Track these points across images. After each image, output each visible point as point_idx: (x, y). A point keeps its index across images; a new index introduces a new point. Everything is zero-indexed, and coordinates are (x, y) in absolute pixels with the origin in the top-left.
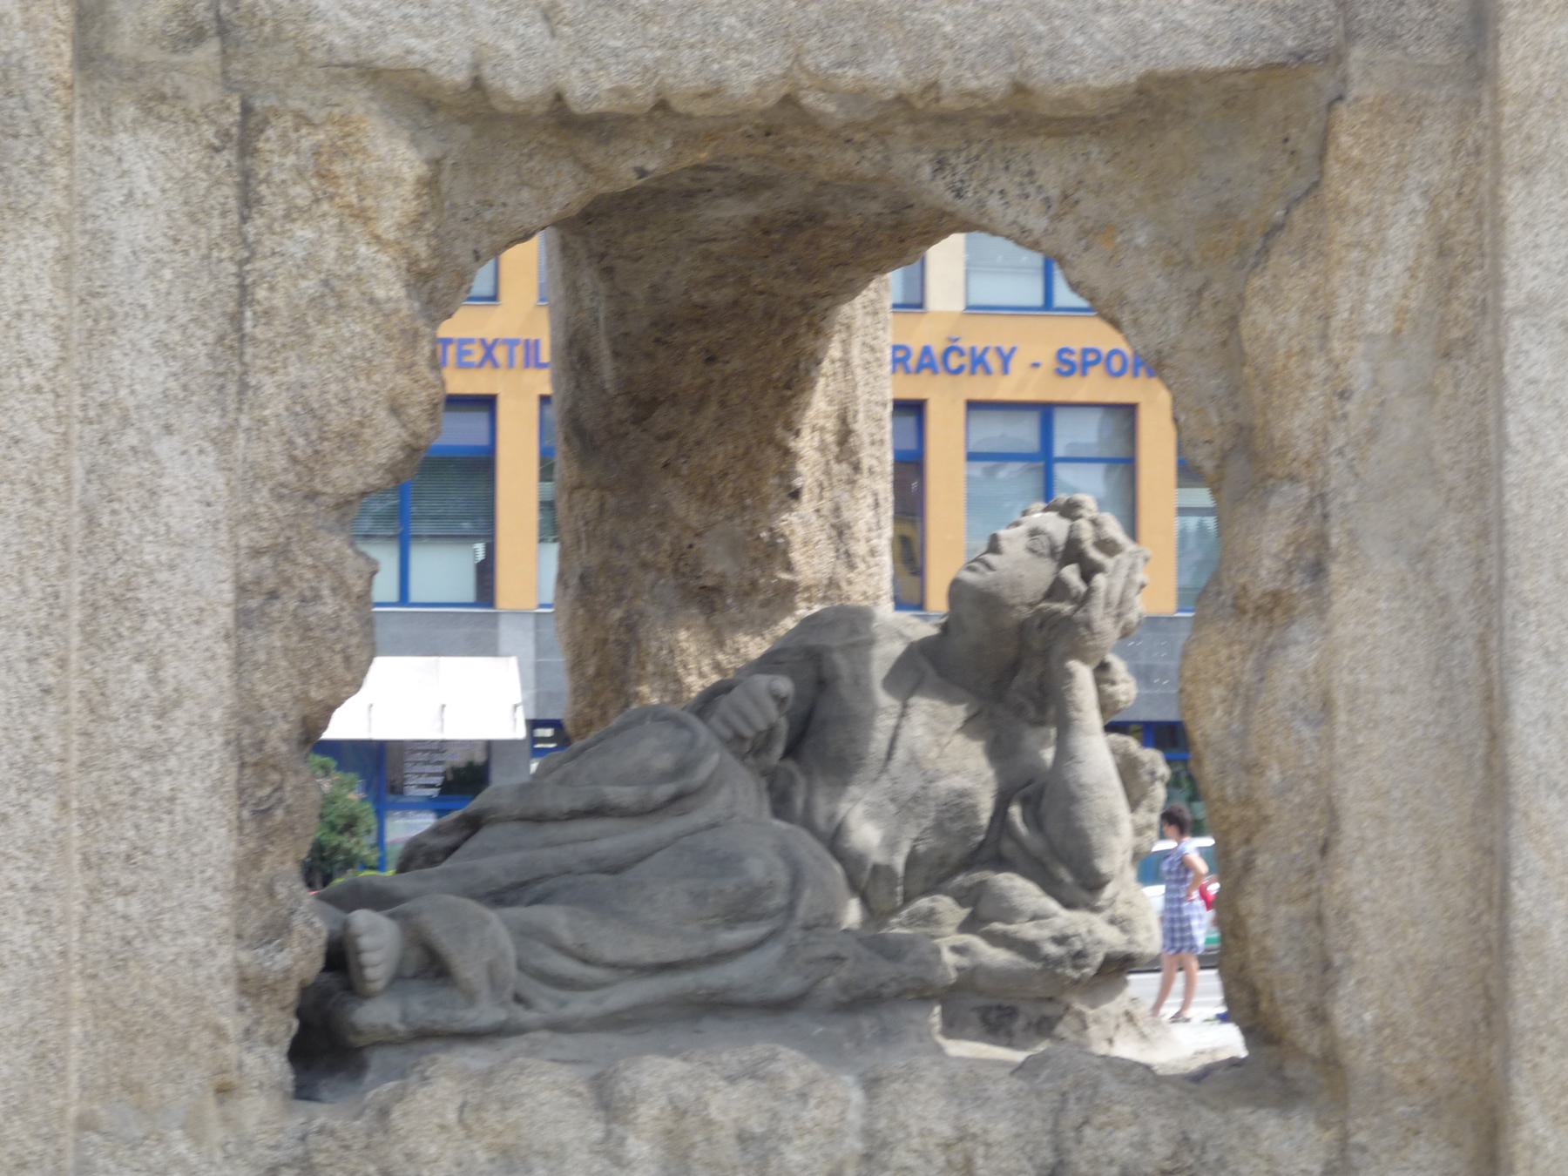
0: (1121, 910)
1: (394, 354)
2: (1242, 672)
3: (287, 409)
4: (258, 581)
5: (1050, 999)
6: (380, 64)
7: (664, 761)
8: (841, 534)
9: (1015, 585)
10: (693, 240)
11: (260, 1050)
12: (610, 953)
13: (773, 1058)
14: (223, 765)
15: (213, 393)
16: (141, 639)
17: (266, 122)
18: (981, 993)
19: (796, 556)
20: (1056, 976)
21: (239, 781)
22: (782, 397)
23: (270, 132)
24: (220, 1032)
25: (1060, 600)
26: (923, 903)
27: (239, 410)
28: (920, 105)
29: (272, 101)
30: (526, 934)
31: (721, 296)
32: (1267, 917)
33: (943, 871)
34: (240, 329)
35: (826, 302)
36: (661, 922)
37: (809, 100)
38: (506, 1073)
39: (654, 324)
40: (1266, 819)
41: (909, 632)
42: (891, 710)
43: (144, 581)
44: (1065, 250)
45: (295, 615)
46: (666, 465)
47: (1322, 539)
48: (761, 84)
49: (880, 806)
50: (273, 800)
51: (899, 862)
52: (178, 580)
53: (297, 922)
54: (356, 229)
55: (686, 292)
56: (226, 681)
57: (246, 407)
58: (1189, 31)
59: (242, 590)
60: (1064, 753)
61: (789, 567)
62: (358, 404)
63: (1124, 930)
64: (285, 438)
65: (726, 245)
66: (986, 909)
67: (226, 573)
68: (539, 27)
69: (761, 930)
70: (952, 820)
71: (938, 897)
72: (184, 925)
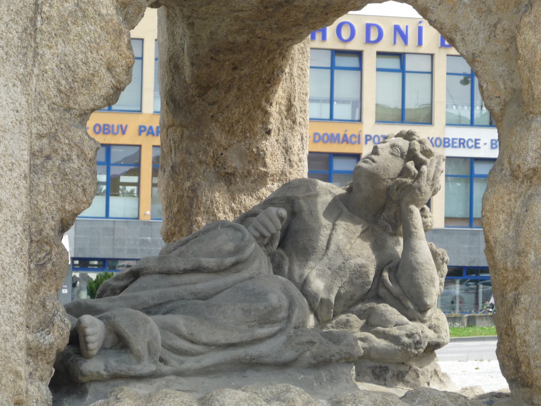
0: (434, 322)
1: (110, 41)
2: (515, 207)
3: (57, 66)
4: (41, 151)
5: (403, 363)
7: (230, 246)
8: (287, 151)
9: (385, 170)
10: (231, 11)
11: (37, 383)
12: (204, 338)
13: (288, 391)
14: (22, 241)
15: (21, 56)
18: (372, 360)
19: (268, 160)
20: (407, 352)
21: (29, 249)
22: (266, 87)
24: (17, 374)
25: (406, 177)
26: (343, 317)
27: (34, 65)
30: (164, 328)
31: (241, 39)
32: (527, 326)
33: (352, 302)
34: (35, 25)
35: (290, 42)
36: (228, 325)
38: (158, 397)
39: (211, 50)
40: (527, 278)
41: (334, 191)
42: (328, 226)
44: (429, 5)
45: (59, 168)
46: (212, 117)
49: (323, 271)
50: (46, 259)
51: (333, 298)
53: (57, 320)
55: (226, 36)
56: (24, 200)
57: (37, 65)
59: (33, 154)
60: (408, 247)
61: (265, 165)
62: (92, 65)
64: (55, 81)
65: (246, 13)
66: (374, 320)
67: (25, 146)
69: (276, 328)
70: (356, 278)
71: (350, 314)
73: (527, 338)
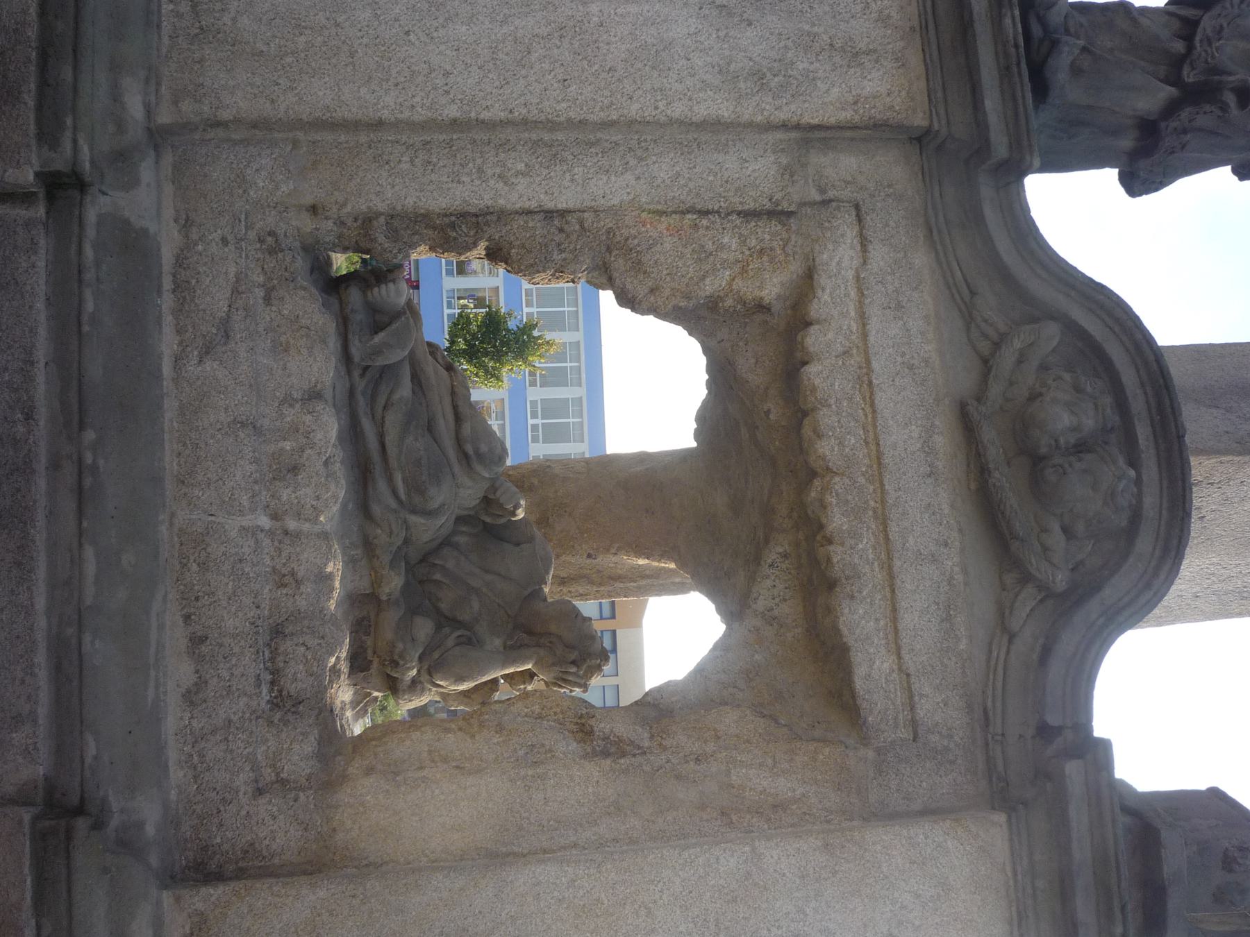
6: (816, 276)
16: (537, 167)
17: (784, 225)
23: (779, 227)
24: (344, 205)
28: (819, 538)
29: (794, 228)
34: (688, 212)
37: (817, 483)
43: (565, 168)
47: (623, 754)
48: (823, 458)
52: (566, 183)
54: (737, 269)
56: (518, 206)
58: (871, 667)
63: (410, 687)
68: (840, 349)
69: (403, 497)
72: (397, 188)
73: (408, 743)
